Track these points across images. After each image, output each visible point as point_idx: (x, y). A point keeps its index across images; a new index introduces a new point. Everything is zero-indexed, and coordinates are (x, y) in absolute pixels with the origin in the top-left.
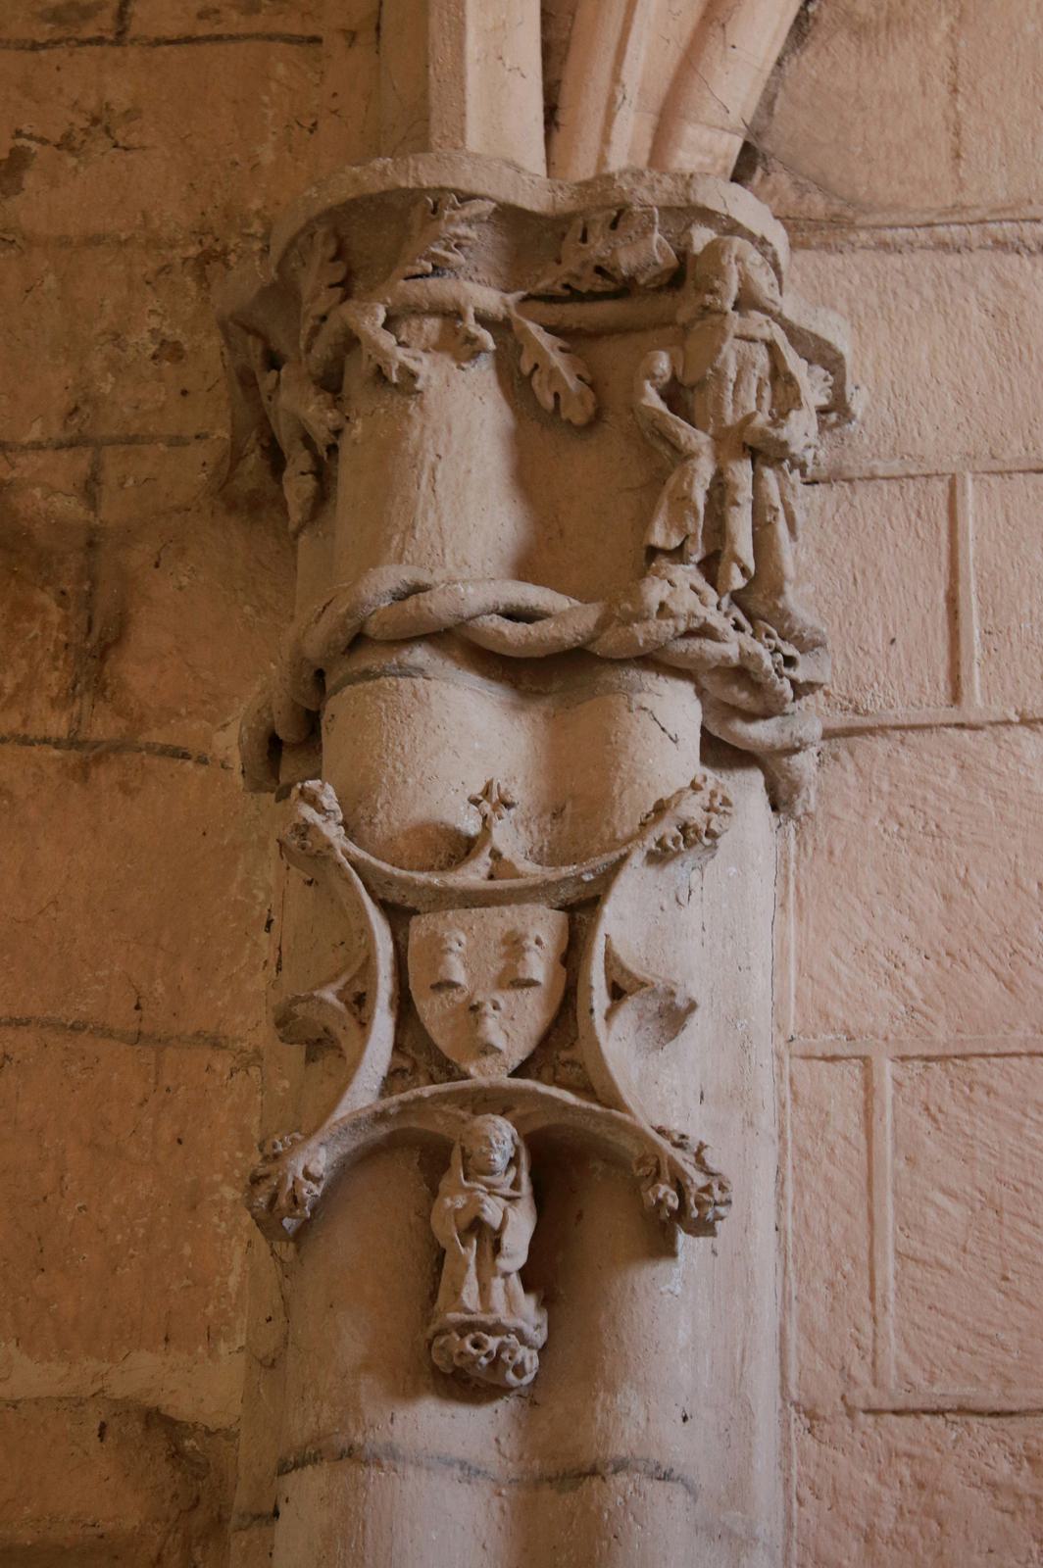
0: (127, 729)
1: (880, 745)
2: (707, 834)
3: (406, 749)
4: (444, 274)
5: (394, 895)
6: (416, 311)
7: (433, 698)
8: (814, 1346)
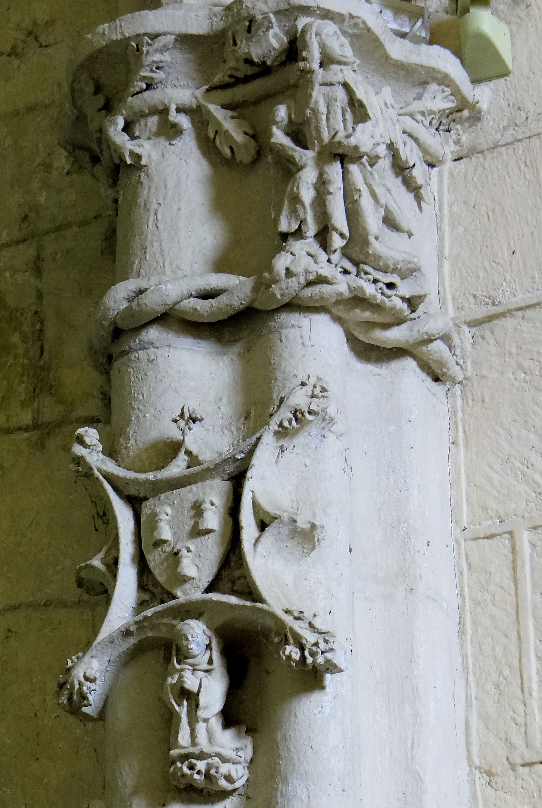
0: (65, 411)
1: (509, 323)
2: (309, 413)
3: (145, 396)
4: (157, 87)
5: (132, 491)
6: (142, 115)
7: (160, 360)
8: (488, 728)
